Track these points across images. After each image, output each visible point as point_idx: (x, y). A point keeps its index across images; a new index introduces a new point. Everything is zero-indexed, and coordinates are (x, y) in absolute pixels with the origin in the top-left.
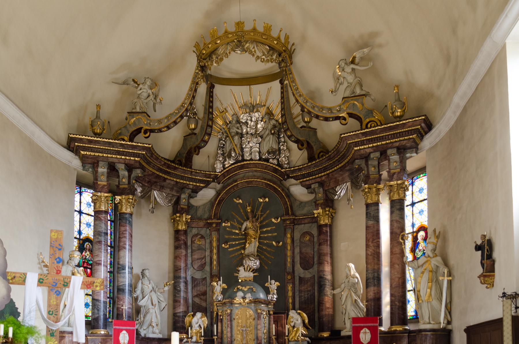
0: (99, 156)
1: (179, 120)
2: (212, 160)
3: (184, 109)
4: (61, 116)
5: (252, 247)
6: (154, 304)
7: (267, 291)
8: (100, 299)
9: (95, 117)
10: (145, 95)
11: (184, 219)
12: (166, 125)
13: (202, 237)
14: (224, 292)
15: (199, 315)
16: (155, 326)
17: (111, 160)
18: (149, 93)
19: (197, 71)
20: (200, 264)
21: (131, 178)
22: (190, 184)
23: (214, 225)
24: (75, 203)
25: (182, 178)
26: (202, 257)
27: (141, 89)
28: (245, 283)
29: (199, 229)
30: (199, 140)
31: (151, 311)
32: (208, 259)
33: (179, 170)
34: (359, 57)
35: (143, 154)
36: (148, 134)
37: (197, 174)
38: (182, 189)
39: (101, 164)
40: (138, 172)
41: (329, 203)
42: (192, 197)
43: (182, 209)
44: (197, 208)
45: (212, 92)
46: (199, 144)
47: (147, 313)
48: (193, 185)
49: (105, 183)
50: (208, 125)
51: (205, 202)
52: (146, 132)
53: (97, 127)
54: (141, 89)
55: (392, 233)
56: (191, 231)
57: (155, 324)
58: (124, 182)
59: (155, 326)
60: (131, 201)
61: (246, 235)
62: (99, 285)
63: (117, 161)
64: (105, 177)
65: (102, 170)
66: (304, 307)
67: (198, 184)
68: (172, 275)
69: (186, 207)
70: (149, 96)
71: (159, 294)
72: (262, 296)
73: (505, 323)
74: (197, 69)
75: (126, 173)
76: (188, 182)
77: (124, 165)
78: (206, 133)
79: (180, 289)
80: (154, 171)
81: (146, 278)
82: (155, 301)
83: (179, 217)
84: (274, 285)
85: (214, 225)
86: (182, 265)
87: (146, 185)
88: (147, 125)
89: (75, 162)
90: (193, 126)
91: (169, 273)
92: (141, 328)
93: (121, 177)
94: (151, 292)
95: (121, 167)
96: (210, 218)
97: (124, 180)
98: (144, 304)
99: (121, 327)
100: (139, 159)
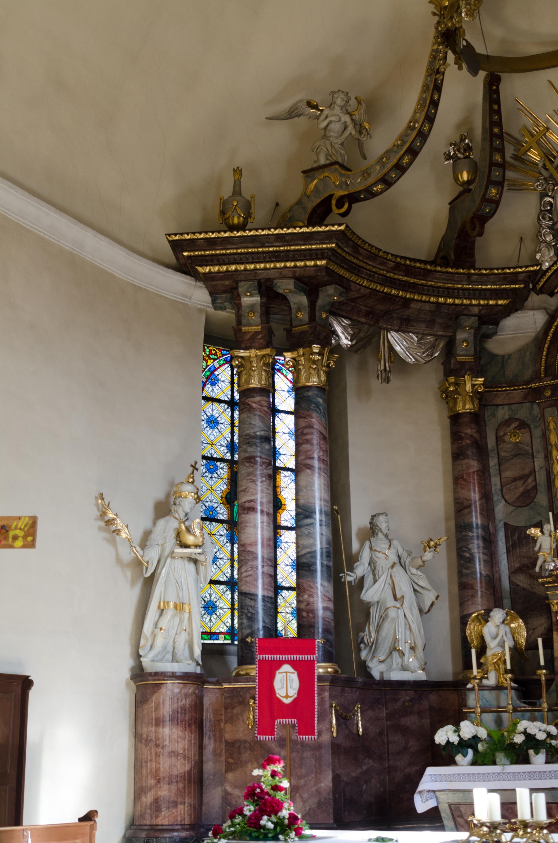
0: (236, 270)
1: (406, 160)
2: (529, 246)
3: (415, 133)
4: (159, 204)
6: (398, 596)
8: (252, 591)
9: (231, 194)
10: (336, 127)
11: (468, 388)
12: (380, 176)
13: (523, 425)
16: (407, 651)
17: (263, 275)
18: (345, 122)
19: (435, 47)
20: (521, 489)
21: (317, 308)
22: (471, 305)
23: (548, 393)
25: (449, 293)
26: (527, 472)
27: (326, 117)
29: (513, 407)
30: (478, 200)
31: (392, 613)
32: (541, 477)
33: (437, 275)
35: (332, 249)
36: (346, 206)
37: (484, 279)
38: (456, 318)
39: (243, 287)
40: (330, 294)
42: (490, 336)
43: (462, 363)
44: (504, 360)
45: (497, 92)
46: (479, 209)
47: (383, 618)
48: (479, 305)
49: (258, 328)
50: (492, 164)
51: (522, 343)
52: (340, 205)
53: (233, 210)
54: (326, 117)
56: (494, 415)
57: (408, 646)
58: (301, 320)
59: (407, 651)
60: (317, 357)
62: (21, 533)
63: (277, 275)
64: (258, 314)
65: (250, 299)
67: (491, 302)
68: (452, 524)
69: (471, 359)
70: (346, 128)
71: (414, 571)
74: (436, 42)
75: (304, 300)
76: (466, 302)
77: (292, 281)
78: (490, 183)
79: (472, 555)
80: (373, 286)
81: (380, 535)
82: (404, 587)
83: (456, 384)
85: (548, 393)
86: (475, 496)
87: (363, 320)
88: (340, 187)
89: (200, 296)
90: (465, 176)
91: (447, 519)
92: (373, 657)
93: (294, 311)
94: (392, 567)
95: (285, 286)
96: (537, 377)
97: (300, 315)
98: (376, 599)
99: (277, 657)
100: (324, 262)
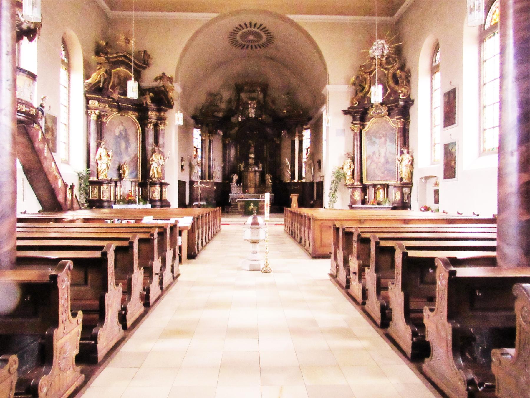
5: (252, 149)
7: (259, 168)
14: (244, 167)
15: (236, 175)
24: (195, 140)
28: (251, 165)
34: (290, 92)
41: (279, 136)
55: (294, 159)
61: (250, 145)
66: (270, 173)
72: (257, 169)
73: (186, 255)
84: (261, 165)
